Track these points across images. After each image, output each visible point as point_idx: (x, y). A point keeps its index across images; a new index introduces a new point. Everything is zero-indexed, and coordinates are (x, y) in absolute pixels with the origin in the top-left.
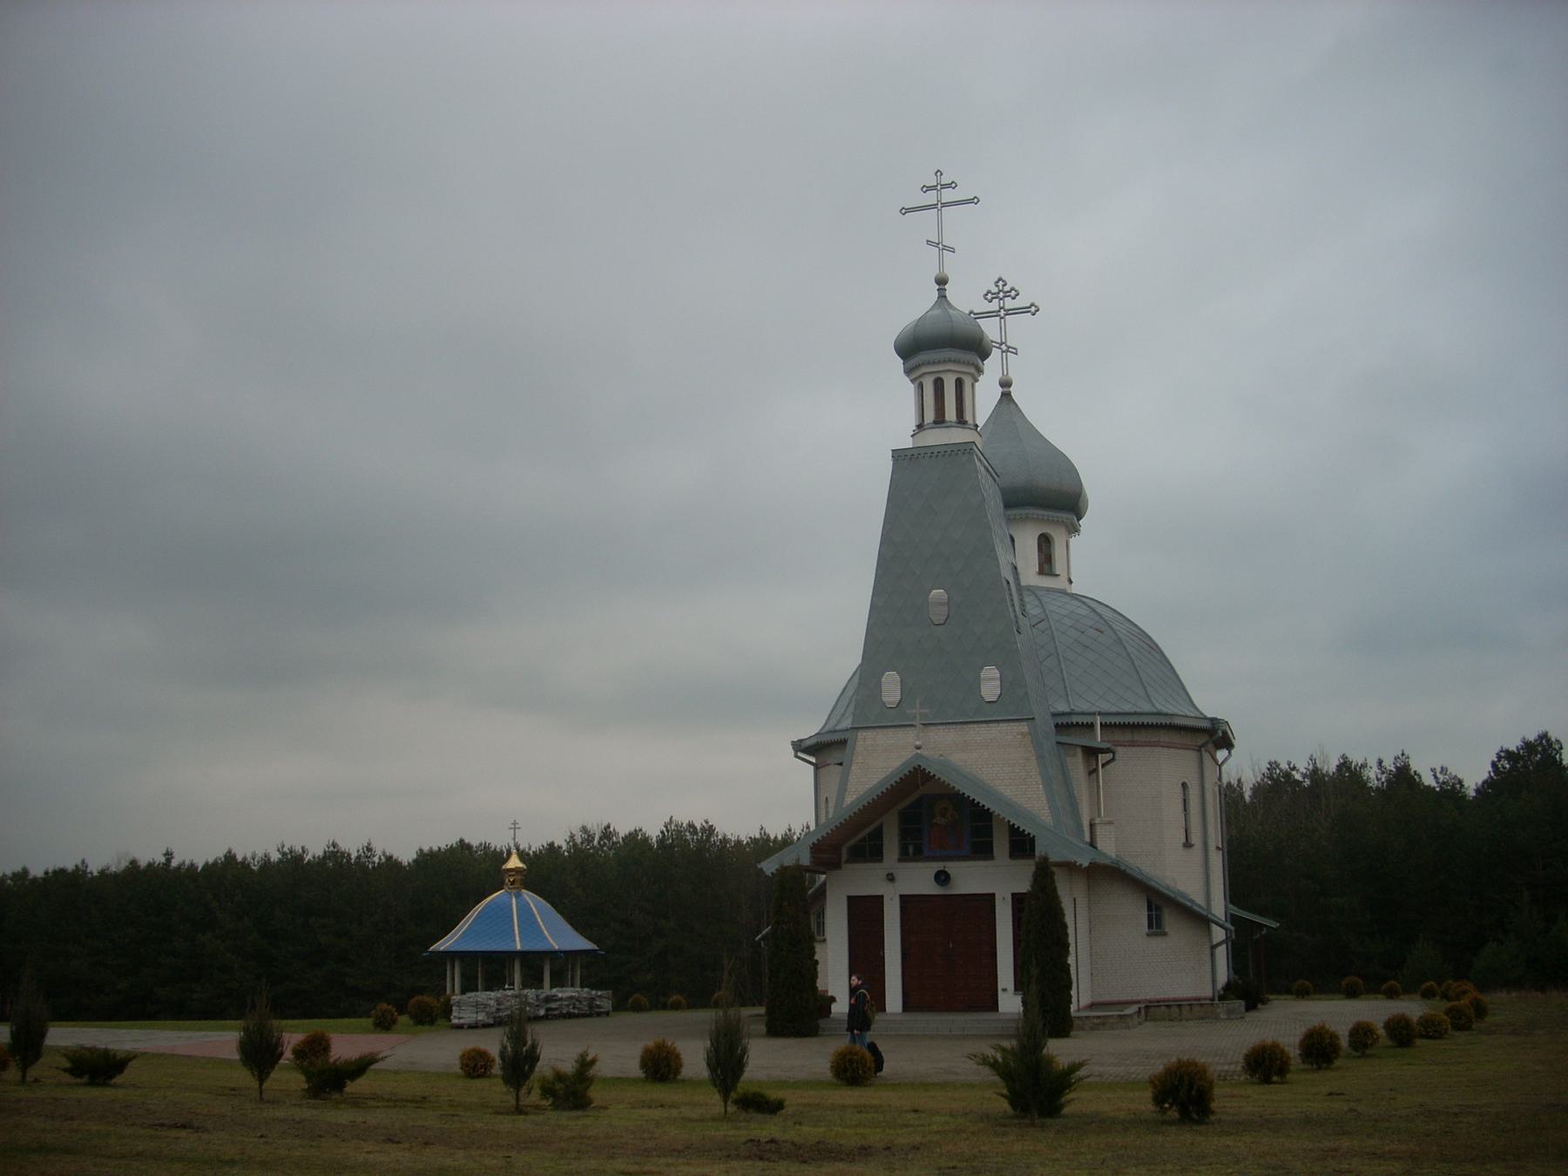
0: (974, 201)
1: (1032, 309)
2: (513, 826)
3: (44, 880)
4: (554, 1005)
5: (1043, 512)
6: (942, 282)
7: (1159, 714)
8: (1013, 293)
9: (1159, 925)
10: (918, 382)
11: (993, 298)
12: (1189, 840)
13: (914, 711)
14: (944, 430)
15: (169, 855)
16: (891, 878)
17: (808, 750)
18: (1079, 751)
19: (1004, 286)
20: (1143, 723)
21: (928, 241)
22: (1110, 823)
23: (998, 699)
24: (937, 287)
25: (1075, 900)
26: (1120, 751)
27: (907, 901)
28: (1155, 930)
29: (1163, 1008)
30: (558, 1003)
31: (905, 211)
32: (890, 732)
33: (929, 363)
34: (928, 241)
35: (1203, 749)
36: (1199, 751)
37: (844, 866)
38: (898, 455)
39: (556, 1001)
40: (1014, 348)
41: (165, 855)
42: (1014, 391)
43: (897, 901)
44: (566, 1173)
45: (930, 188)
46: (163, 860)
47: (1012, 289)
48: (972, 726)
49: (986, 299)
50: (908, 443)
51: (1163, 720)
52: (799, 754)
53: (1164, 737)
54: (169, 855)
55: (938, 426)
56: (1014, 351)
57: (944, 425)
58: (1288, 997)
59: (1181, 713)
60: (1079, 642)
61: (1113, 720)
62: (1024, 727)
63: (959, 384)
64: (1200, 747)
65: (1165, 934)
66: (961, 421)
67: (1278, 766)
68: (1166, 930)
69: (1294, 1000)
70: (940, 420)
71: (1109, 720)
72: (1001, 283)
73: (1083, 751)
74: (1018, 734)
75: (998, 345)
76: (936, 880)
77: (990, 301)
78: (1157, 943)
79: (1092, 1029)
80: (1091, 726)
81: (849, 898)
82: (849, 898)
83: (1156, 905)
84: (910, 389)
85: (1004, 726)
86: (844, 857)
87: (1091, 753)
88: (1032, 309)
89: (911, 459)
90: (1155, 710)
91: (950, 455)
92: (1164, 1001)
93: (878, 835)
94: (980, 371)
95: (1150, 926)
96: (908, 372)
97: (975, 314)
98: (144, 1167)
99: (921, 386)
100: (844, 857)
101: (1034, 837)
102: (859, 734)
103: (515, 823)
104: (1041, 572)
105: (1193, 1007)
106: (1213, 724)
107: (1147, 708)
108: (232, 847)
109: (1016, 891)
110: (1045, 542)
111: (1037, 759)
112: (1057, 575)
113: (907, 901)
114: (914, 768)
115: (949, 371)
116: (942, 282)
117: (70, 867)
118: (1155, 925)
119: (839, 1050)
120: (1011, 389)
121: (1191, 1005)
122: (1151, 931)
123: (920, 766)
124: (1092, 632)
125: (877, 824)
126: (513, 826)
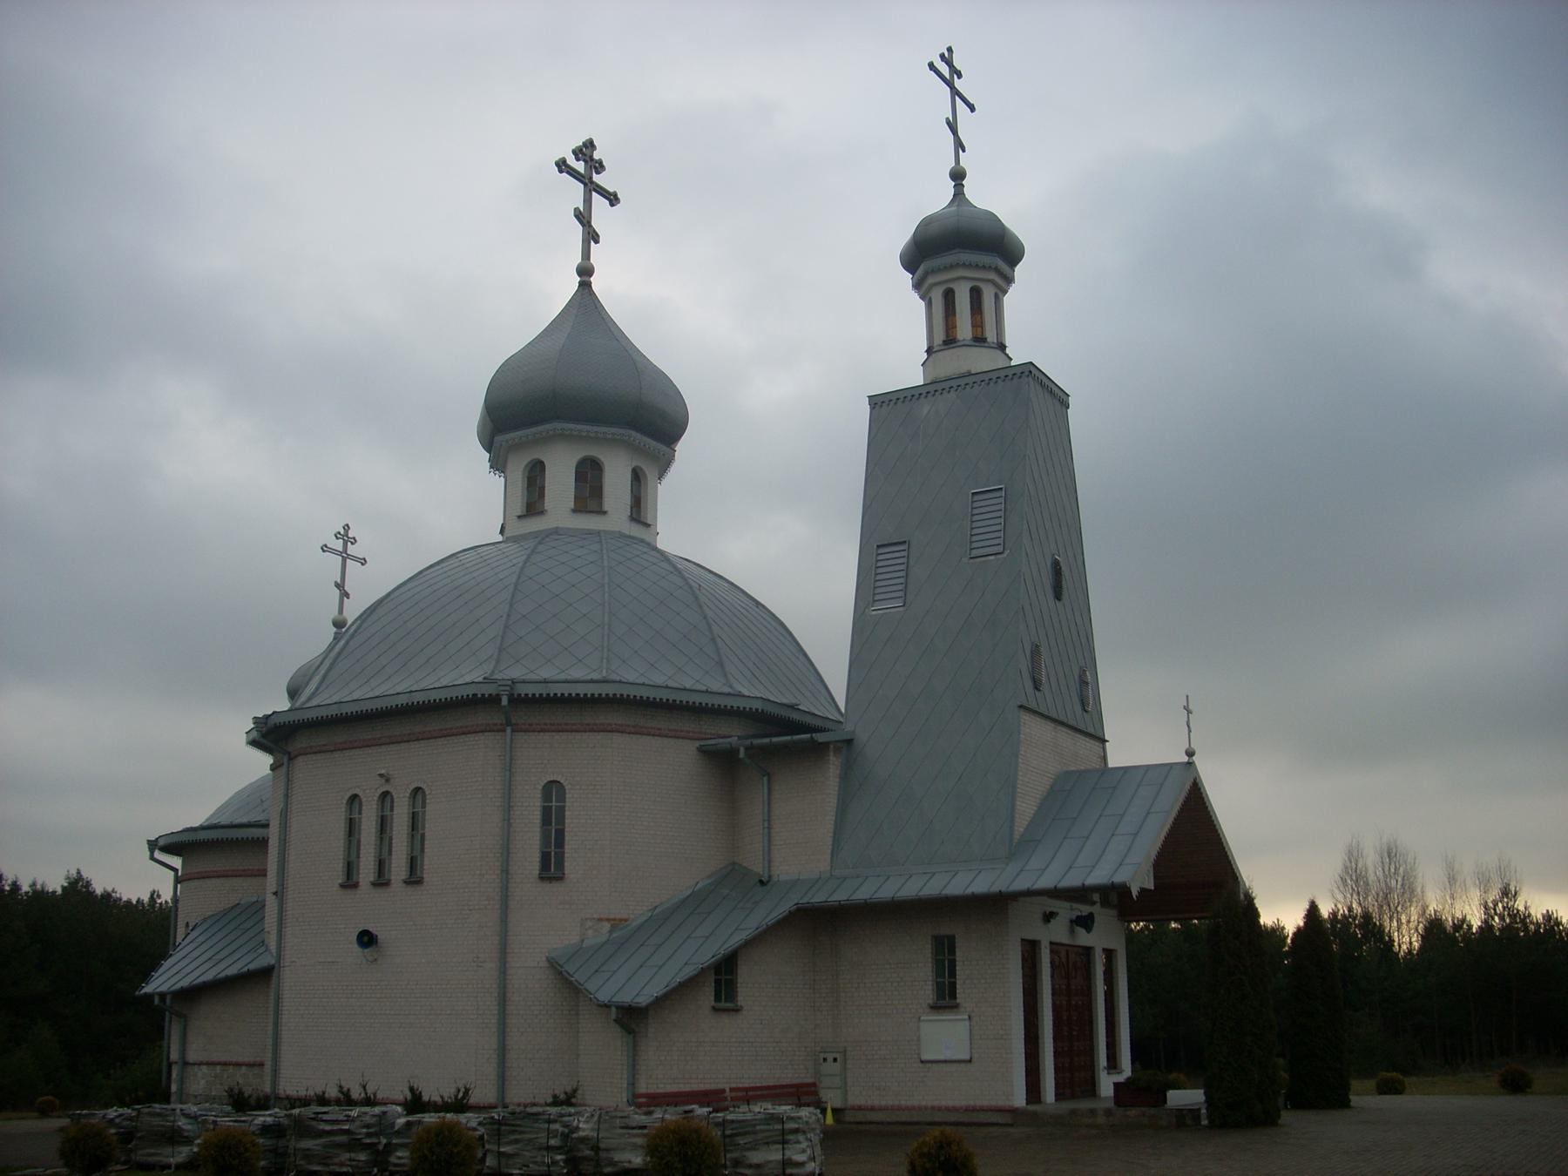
6: (958, 176)
13: (553, 853)
17: (170, 849)
25: (922, 1062)
33: (965, 266)
42: (596, 282)
47: (344, 528)
52: (158, 855)
63: (976, 295)
66: (979, 340)
67: (159, 896)
72: (339, 536)
90: (726, 690)
91: (1020, 377)
94: (1009, 280)
96: (917, 286)
108: (47, 882)
116: (958, 176)
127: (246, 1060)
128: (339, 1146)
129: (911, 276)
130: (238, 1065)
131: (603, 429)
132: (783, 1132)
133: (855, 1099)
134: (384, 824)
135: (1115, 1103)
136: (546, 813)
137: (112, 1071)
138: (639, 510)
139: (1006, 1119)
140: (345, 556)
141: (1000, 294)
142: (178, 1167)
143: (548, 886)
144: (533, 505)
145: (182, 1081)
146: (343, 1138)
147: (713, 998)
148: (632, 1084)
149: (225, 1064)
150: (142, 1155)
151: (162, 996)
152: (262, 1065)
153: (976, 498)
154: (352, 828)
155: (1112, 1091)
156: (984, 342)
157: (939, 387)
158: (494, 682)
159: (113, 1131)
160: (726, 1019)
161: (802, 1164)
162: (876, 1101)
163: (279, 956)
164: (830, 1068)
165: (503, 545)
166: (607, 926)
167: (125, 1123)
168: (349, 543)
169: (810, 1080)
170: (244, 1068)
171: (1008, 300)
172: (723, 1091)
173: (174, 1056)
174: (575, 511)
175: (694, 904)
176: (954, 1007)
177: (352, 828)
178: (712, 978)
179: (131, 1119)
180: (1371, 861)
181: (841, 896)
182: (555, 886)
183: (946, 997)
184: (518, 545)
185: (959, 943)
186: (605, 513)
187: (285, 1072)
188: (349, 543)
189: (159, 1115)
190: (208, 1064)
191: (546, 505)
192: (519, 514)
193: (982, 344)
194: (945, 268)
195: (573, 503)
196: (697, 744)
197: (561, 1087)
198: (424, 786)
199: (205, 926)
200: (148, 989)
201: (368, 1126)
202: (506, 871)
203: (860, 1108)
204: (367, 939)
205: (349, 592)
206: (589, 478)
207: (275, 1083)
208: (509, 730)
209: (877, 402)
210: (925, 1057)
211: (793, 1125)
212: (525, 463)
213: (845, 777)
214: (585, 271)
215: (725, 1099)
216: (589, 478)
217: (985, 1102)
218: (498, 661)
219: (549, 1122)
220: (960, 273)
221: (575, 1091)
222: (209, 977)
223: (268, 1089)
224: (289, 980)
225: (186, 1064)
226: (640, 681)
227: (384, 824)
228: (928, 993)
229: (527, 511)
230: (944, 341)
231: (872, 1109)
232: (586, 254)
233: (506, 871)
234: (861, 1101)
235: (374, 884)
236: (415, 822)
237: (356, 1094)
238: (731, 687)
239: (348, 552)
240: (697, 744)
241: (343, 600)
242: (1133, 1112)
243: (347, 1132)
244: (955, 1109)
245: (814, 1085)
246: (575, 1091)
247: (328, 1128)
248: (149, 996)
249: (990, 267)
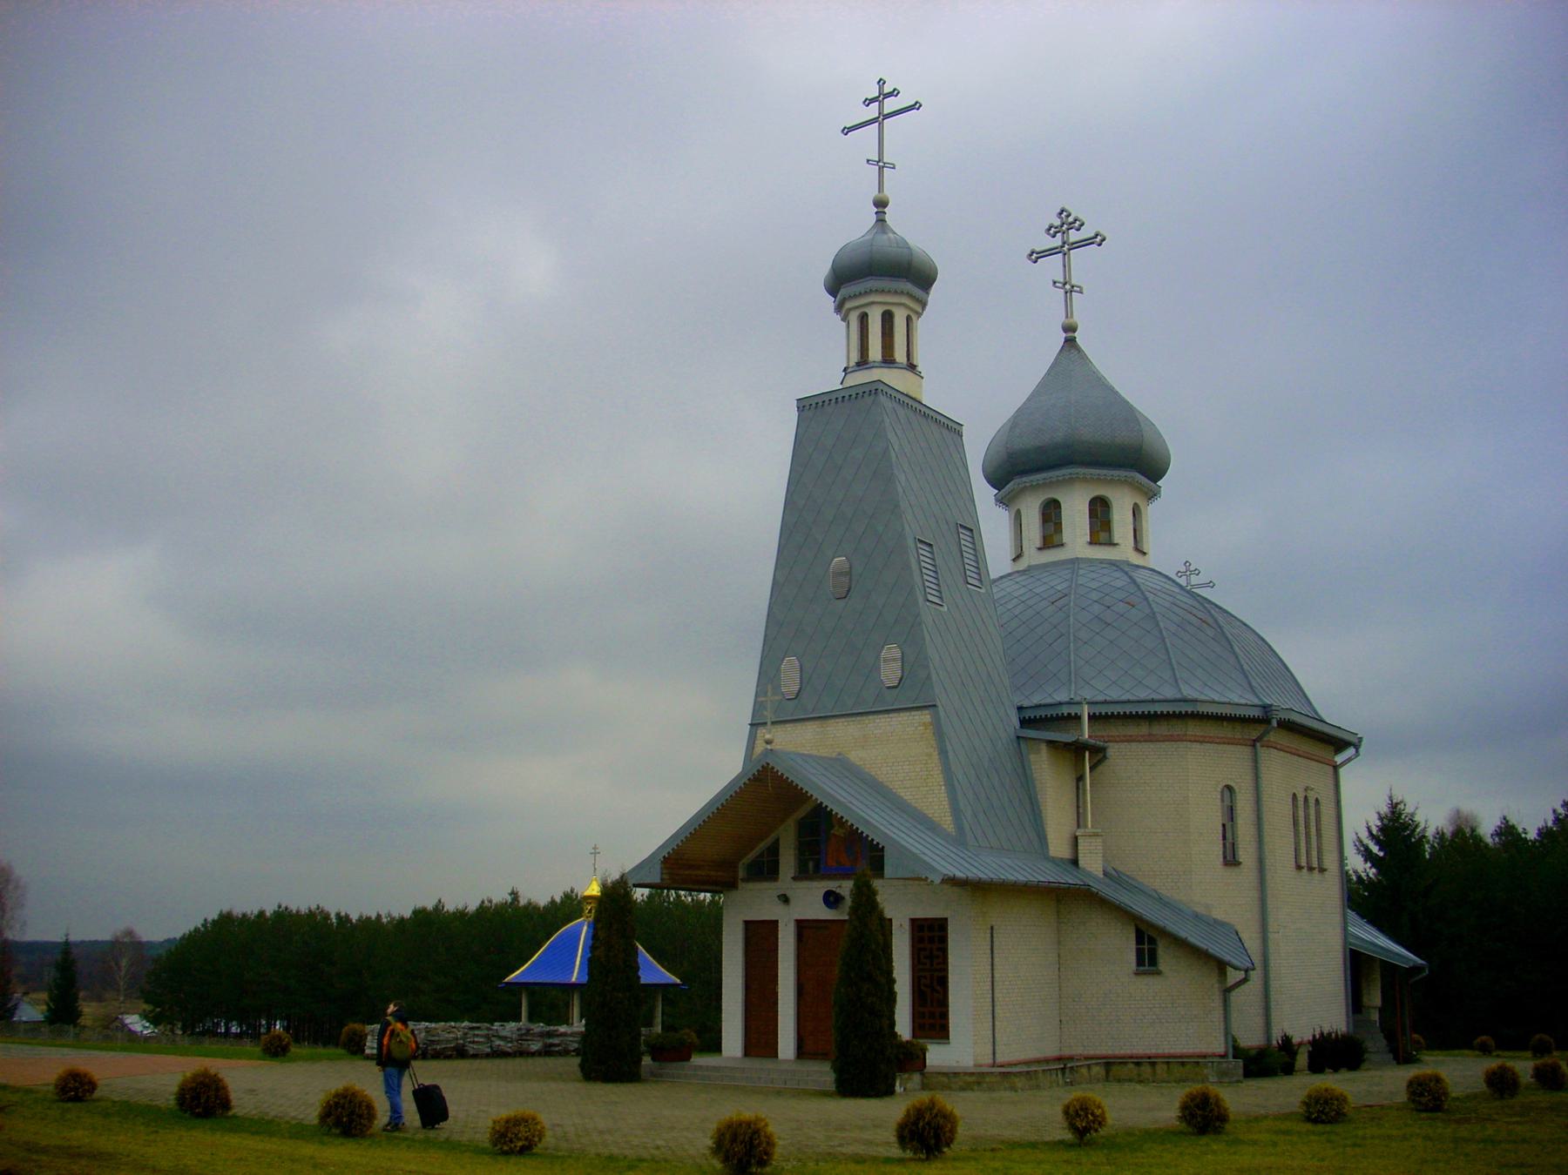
0: (916, 106)
1: (1097, 240)
2: (593, 851)
3: (454, 913)
4: (556, 1041)
5: (1098, 471)
6: (881, 204)
7: (1185, 700)
8: (1077, 224)
9: (1153, 961)
11: (1056, 232)
12: (1236, 856)
14: (865, 371)
15: (514, 894)
16: (785, 899)
18: (1043, 747)
20: (1180, 712)
21: (894, 168)
22: (1096, 835)
23: (899, 684)
24: (876, 210)
25: (992, 928)
26: (1113, 750)
27: (802, 926)
28: (1146, 968)
29: (1131, 1066)
30: (561, 1038)
31: (847, 131)
32: (789, 727)
34: (868, 161)
35: (1258, 744)
36: (1254, 746)
37: (741, 885)
38: (810, 408)
39: (558, 1036)
40: (1078, 287)
41: (510, 894)
42: (1079, 336)
43: (907, 926)
45: (872, 100)
46: (509, 899)
47: (1076, 220)
48: (871, 717)
49: (1049, 234)
51: (1189, 708)
53: (1193, 729)
54: (514, 894)
55: (861, 368)
56: (1078, 289)
57: (868, 366)
58: (331, 1051)
59: (1207, 698)
60: (1099, 618)
61: (1104, 710)
62: (926, 717)
63: (909, 319)
64: (1254, 741)
65: (1159, 973)
66: (912, 367)
68: (1160, 968)
69: (1478, 1056)
70: (888, 360)
71: (1098, 710)
73: (1047, 746)
74: (920, 726)
75: (1075, 288)
76: (825, 903)
77: (1054, 237)
78: (1148, 986)
79: (963, 1089)
80: (1078, 718)
81: (747, 923)
82: (747, 923)
83: (1148, 936)
85: (904, 716)
86: (741, 874)
87: (1076, 750)
88: (1097, 240)
89: (816, 407)
90: (1179, 696)
92: (1131, 1057)
93: (774, 851)
94: (924, 305)
95: (1140, 962)
97: (1037, 253)
100: (741, 874)
101: (883, 847)
102: (758, 732)
103: (595, 848)
104: (1093, 542)
105: (1171, 1066)
106: (1266, 712)
107: (1169, 693)
109: (799, 918)
111: (939, 754)
112: (1117, 544)
113: (802, 926)
114: (763, 767)
115: (873, 303)
116: (881, 204)
117: (430, 906)
118: (1147, 960)
119: (918, 1105)
120: (1076, 334)
121: (1168, 1063)
122: (1142, 968)
123: (768, 764)
124: (1121, 607)
125: (770, 840)
126: (593, 851)
129: (833, 299)
131: (1104, 472)
141: (914, 317)
155: (420, 1121)
156: (867, 363)
171: (920, 325)
174: (1091, 543)
180: (1440, 829)
184: (1027, 577)
191: (1064, 538)
192: (1038, 546)
193: (891, 366)
194: (876, 291)
195: (1089, 537)
198: (1229, 783)
206: (1100, 511)
214: (1070, 329)
216: (1100, 511)
220: (904, 300)
226: (1124, 698)
229: (1044, 545)
230: (857, 363)
232: (1068, 312)
238: (1260, 699)
249: (860, 293)
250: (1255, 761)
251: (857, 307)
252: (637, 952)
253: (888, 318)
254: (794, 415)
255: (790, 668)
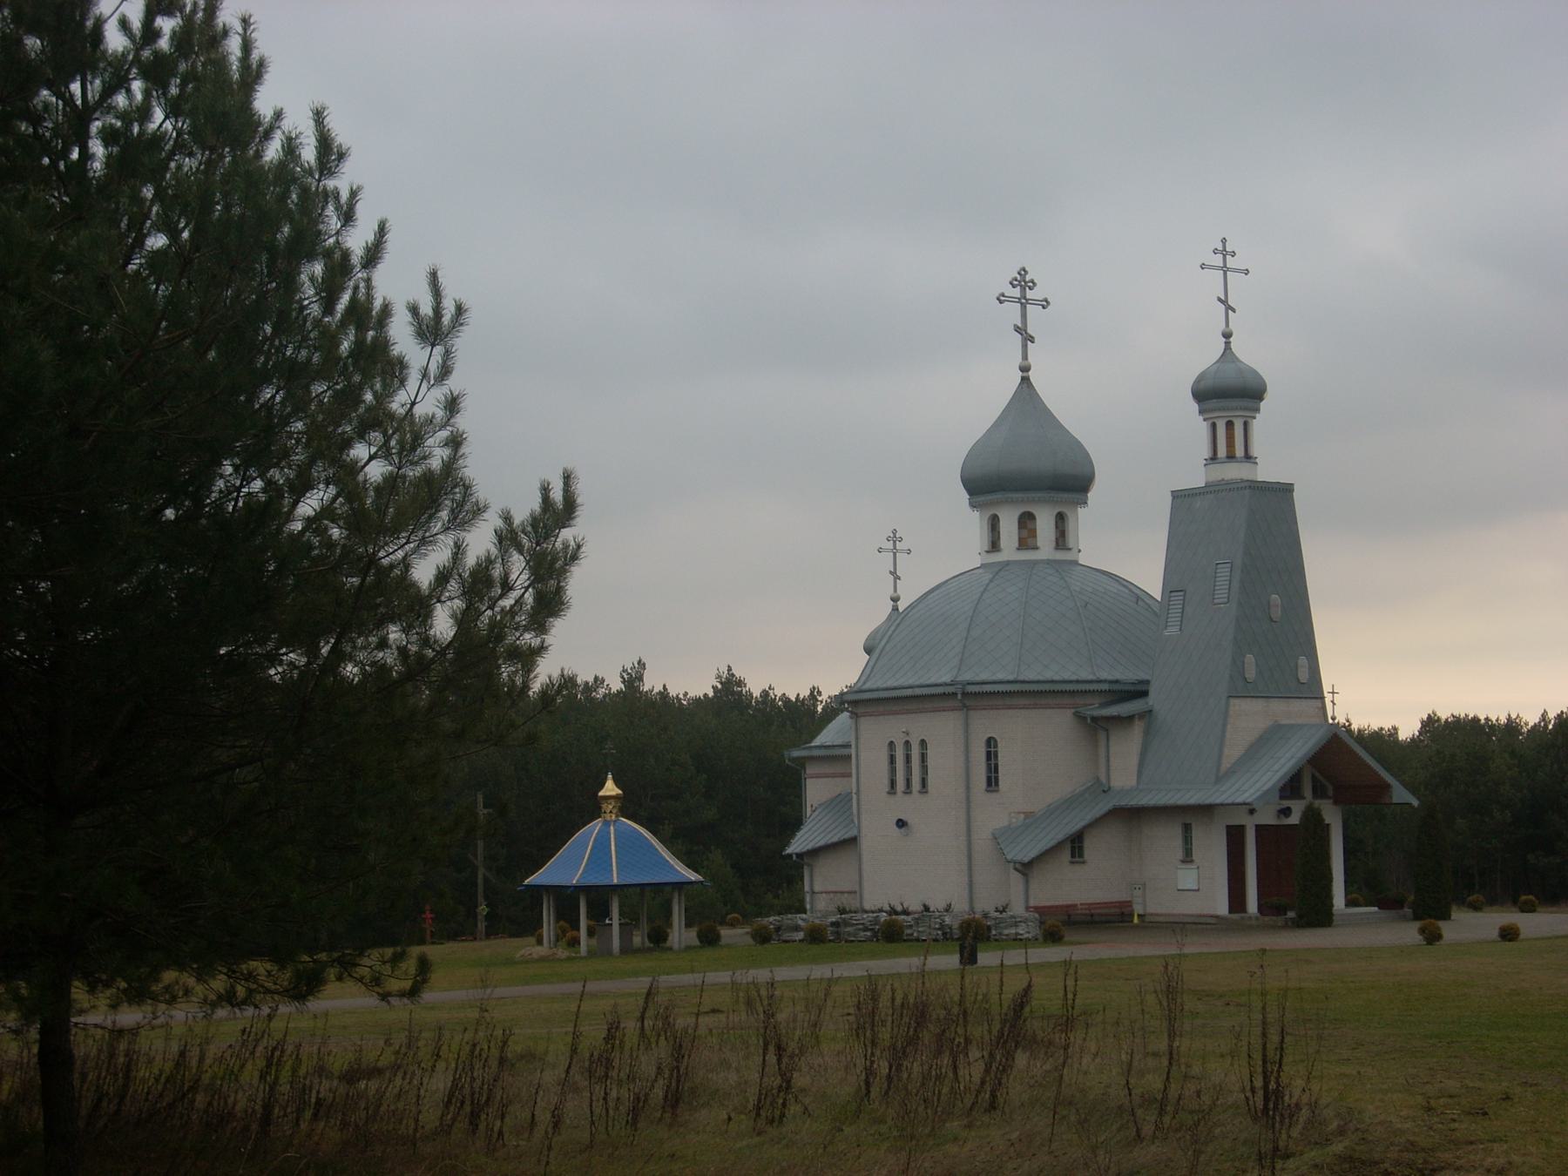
6: (1227, 335)
10: (1210, 422)
19: (1016, 280)
23: (1227, 705)
24: (1224, 340)
25: (1179, 890)
27: (1259, 828)
44: (1489, 1171)
47: (1019, 273)
50: (1196, 477)
57: (1234, 460)
66: (1248, 457)
70: (1231, 456)
81: (1227, 826)
84: (1202, 428)
98: (351, 1129)
99: (1214, 426)
110: (1061, 518)
112: (1070, 549)
113: (1259, 828)
116: (1227, 335)
120: (1030, 373)
127: (846, 890)
128: (860, 929)
130: (842, 893)
132: (1016, 922)
133: (1150, 910)
134: (908, 759)
135: (1259, 909)
136: (989, 754)
137: (780, 892)
138: (1061, 541)
139: (1213, 921)
140: (1024, 302)
142: (800, 941)
143: (989, 795)
144: (995, 546)
145: (812, 904)
146: (861, 927)
147: (1070, 856)
148: (1027, 901)
149: (836, 892)
150: (786, 936)
151: (798, 855)
152: (855, 892)
153: (1173, 594)
154: (892, 760)
155: (978, 957)
157: (1208, 489)
158: (958, 683)
159: (772, 927)
160: (1077, 867)
161: (1021, 935)
162: (1159, 911)
163: (859, 832)
164: (1137, 893)
165: (981, 571)
166: (1022, 816)
167: (777, 923)
168: (1027, 288)
169: (1129, 899)
170: (846, 895)
172: (1076, 905)
173: (807, 888)
175: (1069, 803)
176: (1192, 861)
177: (892, 760)
178: (1069, 846)
179: (779, 921)
181: (1134, 803)
182: (994, 795)
183: (1188, 857)
185: (1194, 826)
186: (1037, 548)
187: (866, 896)
188: (1027, 288)
189: (791, 919)
190: (826, 893)
196: (1073, 710)
197: (1000, 904)
198: (925, 739)
199: (820, 810)
200: (789, 850)
201: (871, 921)
202: (968, 788)
203: (1152, 915)
204: (901, 824)
205: (1033, 335)
207: (861, 903)
208: (965, 709)
209: (1177, 495)
210: (1180, 888)
211: (1019, 920)
212: (988, 517)
213: (1147, 733)
214: (1025, 369)
215: (1078, 910)
217: (1205, 912)
218: (959, 669)
219: (935, 918)
221: (1007, 905)
222: (822, 843)
223: (858, 905)
224: (866, 844)
225: (813, 892)
227: (908, 759)
228: (1180, 855)
231: (1157, 915)
232: (1025, 357)
233: (968, 788)
234: (1152, 911)
235: (905, 793)
236: (923, 757)
237: (899, 908)
239: (1028, 297)
240: (1073, 710)
241: (1026, 345)
242: (1266, 918)
243: (863, 924)
244: (1192, 916)
245: (1130, 902)
246: (1007, 905)
247: (855, 922)
248: (790, 856)
250: (967, 715)
251: (1211, 418)
252: (531, 886)
253: (1230, 425)
254: (1170, 498)
255: (1304, 675)
